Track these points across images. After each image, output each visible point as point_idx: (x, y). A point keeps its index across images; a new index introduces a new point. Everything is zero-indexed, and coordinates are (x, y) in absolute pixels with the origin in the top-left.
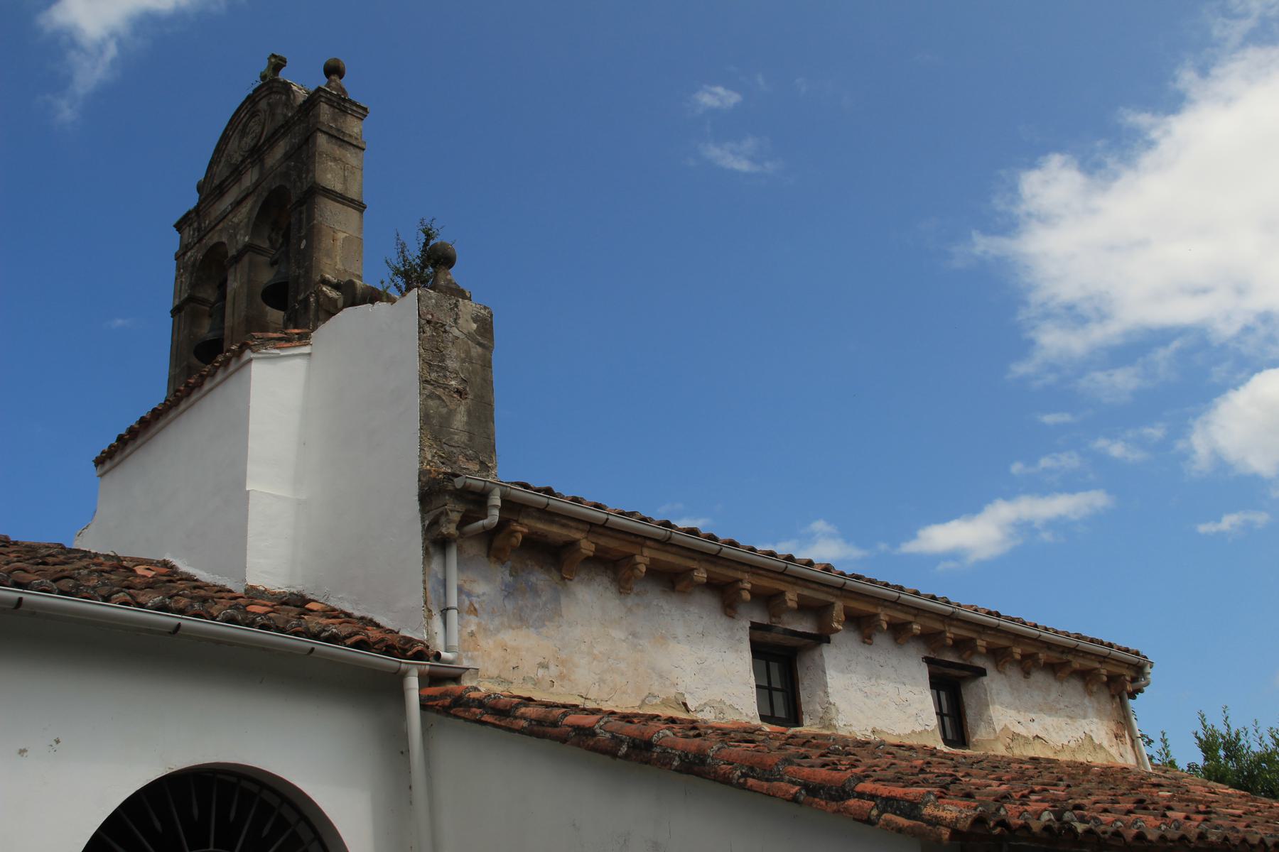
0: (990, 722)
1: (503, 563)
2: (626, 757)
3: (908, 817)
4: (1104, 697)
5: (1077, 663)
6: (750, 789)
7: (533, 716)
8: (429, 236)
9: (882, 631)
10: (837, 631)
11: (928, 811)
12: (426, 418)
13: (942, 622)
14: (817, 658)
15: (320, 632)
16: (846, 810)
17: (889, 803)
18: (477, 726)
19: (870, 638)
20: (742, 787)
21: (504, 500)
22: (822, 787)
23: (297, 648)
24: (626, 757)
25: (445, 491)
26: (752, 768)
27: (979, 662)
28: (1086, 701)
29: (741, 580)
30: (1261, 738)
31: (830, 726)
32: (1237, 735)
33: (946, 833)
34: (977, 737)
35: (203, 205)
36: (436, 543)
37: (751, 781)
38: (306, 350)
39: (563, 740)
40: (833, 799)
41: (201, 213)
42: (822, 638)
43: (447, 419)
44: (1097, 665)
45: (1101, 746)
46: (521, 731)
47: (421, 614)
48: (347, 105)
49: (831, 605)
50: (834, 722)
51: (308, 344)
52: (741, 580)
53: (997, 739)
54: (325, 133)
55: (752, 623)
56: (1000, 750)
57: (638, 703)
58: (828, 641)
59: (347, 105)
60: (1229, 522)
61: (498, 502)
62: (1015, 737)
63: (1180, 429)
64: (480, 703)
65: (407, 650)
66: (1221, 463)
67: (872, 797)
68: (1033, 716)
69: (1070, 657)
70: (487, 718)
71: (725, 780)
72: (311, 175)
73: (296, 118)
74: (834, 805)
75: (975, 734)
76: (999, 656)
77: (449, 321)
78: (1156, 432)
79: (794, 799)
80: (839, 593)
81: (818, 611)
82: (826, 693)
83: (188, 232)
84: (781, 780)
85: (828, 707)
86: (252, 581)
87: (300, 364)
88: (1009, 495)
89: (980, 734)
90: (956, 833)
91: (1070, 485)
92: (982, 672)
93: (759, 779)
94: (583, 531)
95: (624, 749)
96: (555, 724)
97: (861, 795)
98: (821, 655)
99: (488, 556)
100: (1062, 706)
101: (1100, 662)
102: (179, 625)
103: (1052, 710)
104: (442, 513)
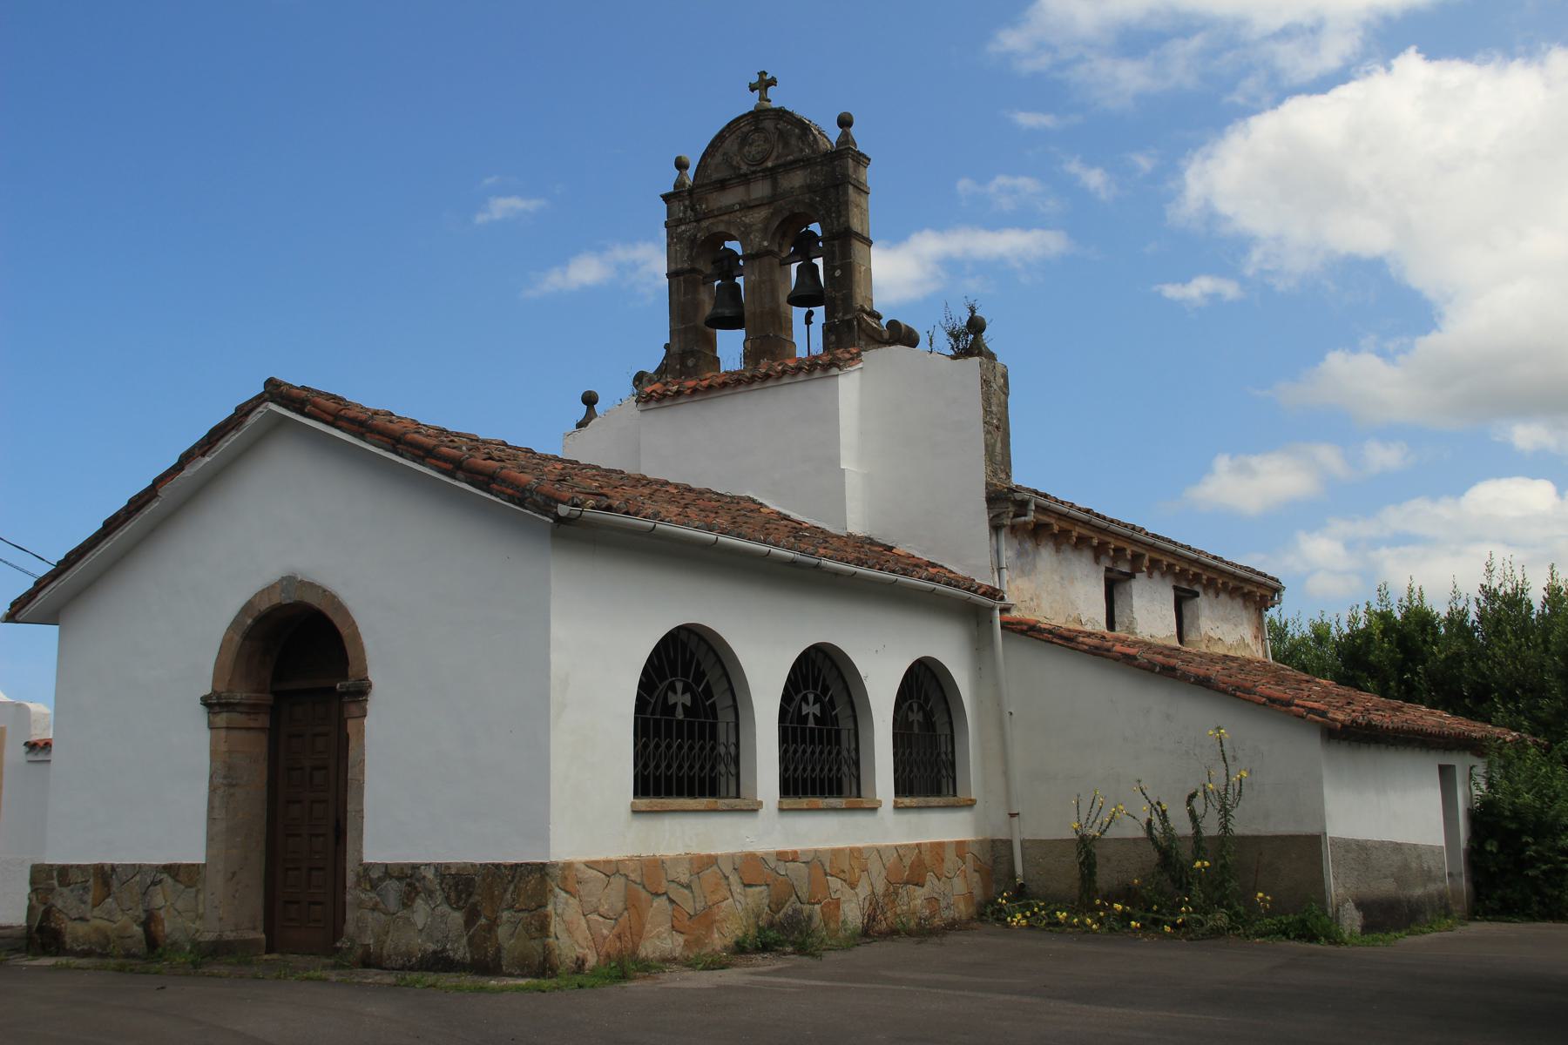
0: (1198, 629)
1: (1016, 537)
2: (1159, 673)
3: (1320, 716)
4: (1252, 610)
5: (1247, 588)
6: (1238, 697)
7: (1092, 644)
8: (973, 310)
9: (1126, 560)
10: (1143, 572)
11: (1330, 715)
12: (987, 446)
13: (1189, 564)
14: (1128, 588)
15: (970, 587)
16: (1291, 711)
17: (1311, 710)
18: (1048, 644)
19: (1151, 574)
20: (1234, 695)
21: (1036, 506)
22: (1279, 700)
23: (926, 587)
24: (1159, 673)
25: (1007, 500)
26: (1238, 687)
27: (1197, 588)
28: (1244, 613)
29: (1109, 543)
30: (1300, 626)
31: (1133, 633)
32: (1286, 623)
33: (1339, 725)
34: (1189, 638)
35: (698, 190)
36: (996, 528)
37: (1238, 693)
38: (860, 365)
39: (1116, 659)
40: (1283, 705)
41: (695, 195)
42: (1131, 576)
43: (994, 446)
44: (1256, 589)
45: (1248, 645)
46: (1084, 651)
47: (990, 570)
48: (861, 158)
49: (1143, 555)
50: (1136, 630)
51: (861, 361)
52: (1109, 543)
53: (1201, 641)
54: (852, 185)
55: (1106, 567)
56: (1204, 649)
57: (1064, 621)
58: (1135, 578)
59: (861, 158)
60: (1200, 287)
61: (1033, 508)
62: (1210, 639)
63: (1171, 167)
64: (1050, 632)
65: (996, 595)
66: (1211, 217)
67: (1303, 707)
68: (1218, 624)
69: (1242, 585)
70: (1055, 640)
71: (1224, 692)
72: (842, 220)
73: (819, 160)
74: (1284, 708)
75: (1188, 636)
76: (1210, 585)
77: (993, 380)
78: (1144, 163)
79: (1264, 704)
80: (1148, 548)
81: (1137, 558)
82: (1132, 611)
83: (679, 209)
84: (1255, 694)
85: (1132, 621)
86: (850, 530)
87: (857, 375)
88: (941, 223)
89: (1191, 636)
90: (1344, 726)
91: (1023, 219)
92: (1196, 595)
93: (1244, 693)
94: (1054, 518)
95: (1158, 669)
96: (1108, 650)
97: (1297, 705)
98: (1131, 586)
99: (1011, 533)
100: (1231, 617)
101: (1258, 588)
102: (935, 588)
103: (1225, 620)
104: (1004, 512)
